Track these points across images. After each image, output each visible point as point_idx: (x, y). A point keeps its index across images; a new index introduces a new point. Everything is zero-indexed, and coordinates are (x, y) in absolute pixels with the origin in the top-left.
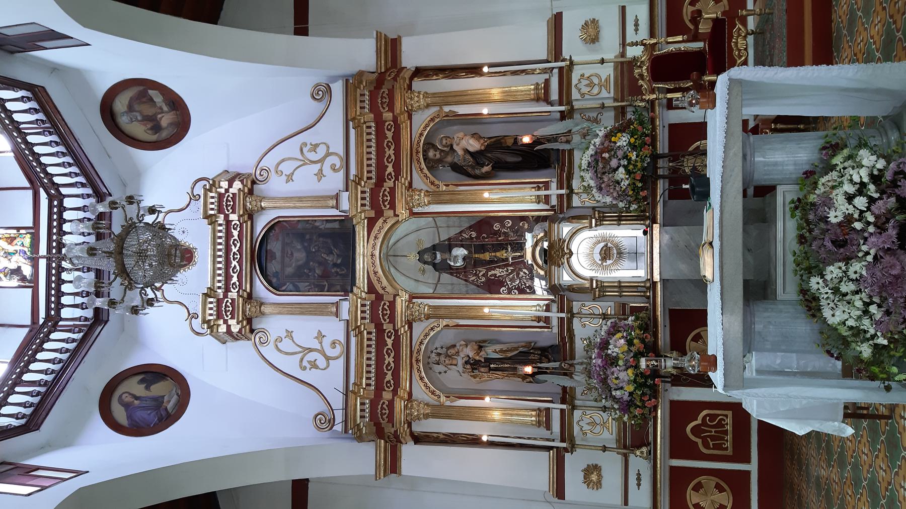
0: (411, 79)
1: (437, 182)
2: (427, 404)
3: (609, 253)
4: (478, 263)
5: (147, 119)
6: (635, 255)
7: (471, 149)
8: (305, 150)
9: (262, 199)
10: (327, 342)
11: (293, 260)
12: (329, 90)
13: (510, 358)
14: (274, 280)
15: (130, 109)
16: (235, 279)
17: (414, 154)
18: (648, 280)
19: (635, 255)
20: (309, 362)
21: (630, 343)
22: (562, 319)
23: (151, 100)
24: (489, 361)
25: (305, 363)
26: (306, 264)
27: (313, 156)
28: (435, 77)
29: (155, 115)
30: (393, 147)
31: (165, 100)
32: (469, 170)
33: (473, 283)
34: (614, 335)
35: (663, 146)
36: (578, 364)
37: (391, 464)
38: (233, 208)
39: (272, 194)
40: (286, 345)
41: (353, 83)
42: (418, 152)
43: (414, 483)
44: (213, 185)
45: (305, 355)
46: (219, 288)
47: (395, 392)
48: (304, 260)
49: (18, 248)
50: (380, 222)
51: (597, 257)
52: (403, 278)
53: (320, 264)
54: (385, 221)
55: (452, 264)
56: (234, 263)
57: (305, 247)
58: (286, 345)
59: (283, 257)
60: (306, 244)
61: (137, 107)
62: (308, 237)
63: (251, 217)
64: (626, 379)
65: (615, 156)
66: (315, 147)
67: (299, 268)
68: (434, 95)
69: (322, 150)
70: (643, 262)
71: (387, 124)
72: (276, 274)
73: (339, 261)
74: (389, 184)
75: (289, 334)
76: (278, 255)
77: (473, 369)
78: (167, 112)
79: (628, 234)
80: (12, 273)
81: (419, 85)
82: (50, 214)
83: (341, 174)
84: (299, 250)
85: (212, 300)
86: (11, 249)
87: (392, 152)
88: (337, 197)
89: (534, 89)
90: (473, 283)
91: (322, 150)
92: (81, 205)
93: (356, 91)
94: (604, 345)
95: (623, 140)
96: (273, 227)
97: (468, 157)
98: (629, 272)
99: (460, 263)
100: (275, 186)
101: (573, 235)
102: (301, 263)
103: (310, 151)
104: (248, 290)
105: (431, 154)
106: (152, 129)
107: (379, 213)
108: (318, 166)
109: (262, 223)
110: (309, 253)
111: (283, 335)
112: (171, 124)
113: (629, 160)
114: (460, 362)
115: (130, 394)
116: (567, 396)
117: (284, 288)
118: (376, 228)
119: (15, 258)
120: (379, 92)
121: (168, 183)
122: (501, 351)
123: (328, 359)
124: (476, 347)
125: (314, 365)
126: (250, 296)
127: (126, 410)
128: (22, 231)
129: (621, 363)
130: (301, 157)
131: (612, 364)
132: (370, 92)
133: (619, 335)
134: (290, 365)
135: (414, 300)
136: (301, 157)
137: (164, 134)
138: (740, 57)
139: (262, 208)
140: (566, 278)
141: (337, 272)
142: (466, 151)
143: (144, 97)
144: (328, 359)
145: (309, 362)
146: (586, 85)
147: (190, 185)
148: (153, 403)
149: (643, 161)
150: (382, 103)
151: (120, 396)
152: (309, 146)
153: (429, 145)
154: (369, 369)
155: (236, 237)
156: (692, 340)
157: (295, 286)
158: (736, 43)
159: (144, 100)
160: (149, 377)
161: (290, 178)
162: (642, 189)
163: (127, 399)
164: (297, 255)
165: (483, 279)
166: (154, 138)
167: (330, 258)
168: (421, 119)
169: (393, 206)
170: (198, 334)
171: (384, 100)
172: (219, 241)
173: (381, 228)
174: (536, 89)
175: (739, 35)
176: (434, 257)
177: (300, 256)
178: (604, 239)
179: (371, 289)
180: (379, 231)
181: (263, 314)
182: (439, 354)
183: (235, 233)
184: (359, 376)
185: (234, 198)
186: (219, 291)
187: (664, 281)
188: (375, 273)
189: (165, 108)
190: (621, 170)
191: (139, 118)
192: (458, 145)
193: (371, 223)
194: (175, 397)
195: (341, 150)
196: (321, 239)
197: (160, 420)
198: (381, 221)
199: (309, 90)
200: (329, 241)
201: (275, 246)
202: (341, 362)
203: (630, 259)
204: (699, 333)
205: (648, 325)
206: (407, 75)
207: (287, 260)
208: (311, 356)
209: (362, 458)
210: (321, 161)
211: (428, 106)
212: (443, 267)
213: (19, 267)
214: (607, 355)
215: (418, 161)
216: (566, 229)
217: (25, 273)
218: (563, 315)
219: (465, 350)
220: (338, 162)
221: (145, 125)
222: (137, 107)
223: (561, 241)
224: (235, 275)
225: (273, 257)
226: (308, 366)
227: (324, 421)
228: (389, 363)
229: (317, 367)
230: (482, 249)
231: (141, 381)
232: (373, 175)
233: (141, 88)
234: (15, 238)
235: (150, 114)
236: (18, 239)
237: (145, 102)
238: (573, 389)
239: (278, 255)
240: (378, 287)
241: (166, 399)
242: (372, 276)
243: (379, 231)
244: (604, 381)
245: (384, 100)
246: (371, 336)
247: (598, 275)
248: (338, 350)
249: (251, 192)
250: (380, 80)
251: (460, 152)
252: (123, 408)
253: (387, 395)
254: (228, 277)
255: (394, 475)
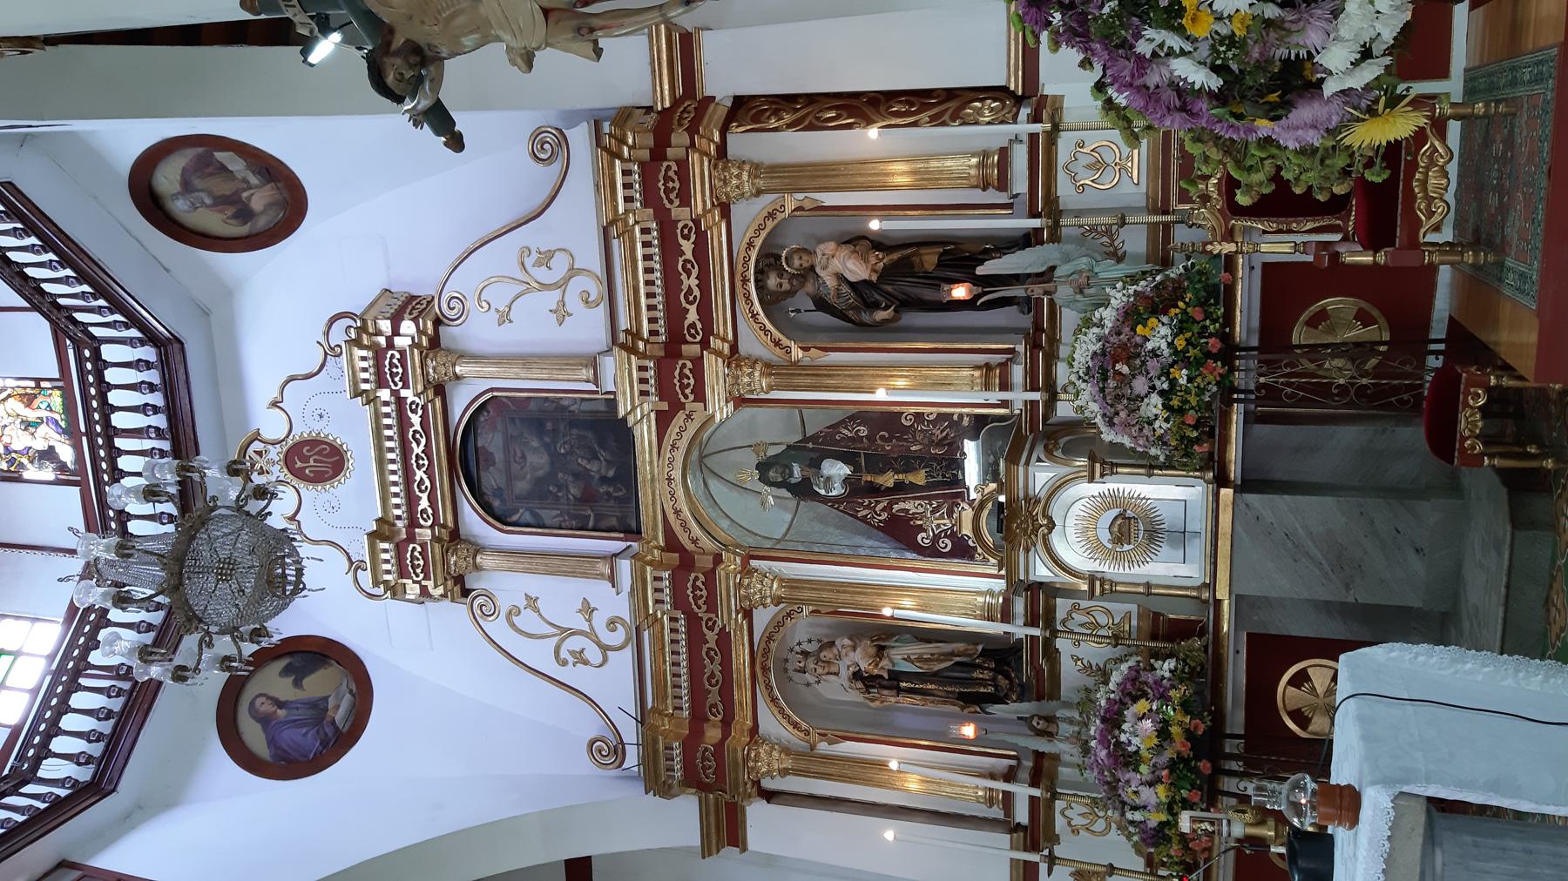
0: (724, 132)
1: (785, 341)
2: (786, 750)
3: (1132, 529)
4: (875, 491)
5: (221, 202)
6: (1181, 537)
7: (852, 279)
8: (529, 262)
9: (463, 356)
10: (599, 621)
11: (527, 468)
12: (563, 140)
13: (936, 674)
14: (496, 503)
15: (187, 187)
16: (424, 503)
17: (738, 284)
18: (1205, 585)
19: (1181, 537)
20: (572, 653)
21: (1163, 733)
22: (1034, 403)
23: (223, 168)
24: (896, 676)
25: (564, 654)
26: (550, 477)
27: (542, 274)
28: (773, 123)
29: (237, 193)
30: (695, 272)
31: (249, 167)
32: (851, 314)
33: (864, 519)
34: (1135, 700)
35: (1246, 321)
36: (1064, 720)
37: (725, 829)
38: (404, 379)
39: (474, 346)
40: (527, 620)
41: (611, 128)
42: (745, 281)
43: (769, 860)
44: (362, 329)
45: (563, 640)
46: (399, 518)
47: (727, 723)
48: (547, 468)
49: (44, 414)
50: (680, 418)
51: (1105, 536)
52: (736, 494)
53: (577, 476)
54: (689, 416)
55: (823, 492)
56: (420, 474)
57: (546, 446)
58: (527, 620)
59: (507, 463)
60: (547, 440)
61: (197, 183)
62: (549, 426)
63: (440, 390)
64: (1153, 800)
65: (1143, 369)
66: (546, 258)
67: (539, 482)
68: (774, 170)
69: (560, 265)
70: (1197, 548)
71: (680, 225)
72: (498, 492)
73: (611, 473)
74: (691, 349)
75: (532, 602)
76: (499, 457)
77: (867, 687)
78: (257, 187)
79: (1171, 495)
80: (41, 458)
81: (743, 143)
82: (82, 373)
83: (601, 312)
84: (535, 450)
85: (385, 546)
86: (31, 415)
87: (693, 282)
88: (593, 362)
89: (978, 166)
90: (864, 519)
91: (560, 265)
92: (86, 729)
93: (612, 167)
94: (1113, 720)
95: (1159, 336)
96: (486, 408)
97: (845, 289)
98: (1172, 569)
99: (838, 490)
100: (476, 330)
101: (1056, 489)
102: (540, 473)
103: (538, 264)
104: (450, 524)
105: (772, 281)
106: (235, 216)
107: (677, 406)
108: (557, 294)
109: (461, 402)
110: (554, 457)
111: (522, 603)
112: (269, 206)
113: (1173, 383)
114: (845, 674)
115: (269, 698)
116: (1042, 770)
117: (515, 518)
118: (673, 430)
119: (43, 429)
120: (665, 145)
121: (280, 331)
122: (920, 659)
123: (605, 649)
124: (872, 651)
125: (580, 658)
126: (455, 535)
127: (265, 728)
128: (43, 384)
129: (1144, 768)
130: (521, 276)
131: (1127, 765)
132: (642, 164)
133: (1142, 706)
134: (540, 655)
135: (754, 563)
136: (521, 276)
137: (262, 223)
138: (1431, 214)
139: (458, 377)
140: (1042, 571)
141: (608, 493)
142: (840, 278)
143: (208, 165)
144: (605, 649)
145: (572, 653)
146: (1089, 167)
147: (322, 327)
148: (310, 713)
149: (1201, 391)
150: (668, 191)
151: (252, 703)
152: (535, 256)
153: (769, 260)
154: (675, 647)
155: (417, 427)
156: (1291, 682)
157: (534, 514)
158: (1424, 183)
159: (210, 170)
160: (297, 661)
161: (504, 318)
162: (1197, 441)
163: (266, 707)
164: (532, 459)
165: (884, 516)
166: (243, 230)
167: (593, 467)
168: (748, 213)
169: (700, 396)
170: (371, 596)
171: (671, 185)
172: (388, 433)
173: (682, 430)
174: (982, 165)
175: (1432, 162)
176: (787, 470)
177: (538, 461)
178: (1113, 500)
179: (672, 543)
180: (680, 434)
181: (477, 568)
182: (805, 654)
183: (415, 419)
184: (660, 694)
185: (403, 361)
186: (400, 524)
187: (1239, 600)
188: (677, 512)
189: (254, 180)
190: (1156, 399)
191: (208, 201)
192: (825, 268)
193: (663, 421)
194: (348, 696)
195: (597, 265)
196: (574, 431)
197: (324, 744)
198: (681, 416)
199: (524, 150)
200: (590, 435)
201: (491, 441)
202: (628, 655)
203: (1173, 544)
204: (1304, 671)
205: (1204, 678)
206: (720, 114)
207: (515, 467)
208: (575, 643)
209: (681, 819)
210: (562, 284)
211: (759, 193)
212: (803, 490)
213: (51, 448)
214: (1118, 744)
215: (748, 298)
216: (1041, 476)
217: (63, 458)
218: (1036, 396)
219: (851, 654)
220: (595, 289)
221: (221, 211)
222: (197, 183)
223: (1032, 500)
224: (424, 496)
225: (491, 461)
226: (571, 660)
227: (608, 751)
228: (712, 675)
229: (586, 663)
230: (879, 463)
231: (286, 671)
232: (661, 326)
233: (200, 150)
234: (35, 396)
235: (228, 193)
236: (40, 399)
237: (211, 174)
238: (1056, 758)
239: (499, 457)
240: (684, 539)
241: (331, 703)
242: (671, 517)
243: (680, 434)
244: (1113, 786)
245: (671, 185)
246: (677, 625)
247: (1106, 569)
248: (618, 637)
249: (435, 342)
250: (663, 123)
251: (831, 282)
252: (258, 726)
253: (713, 734)
254: (412, 501)
255: (730, 852)
